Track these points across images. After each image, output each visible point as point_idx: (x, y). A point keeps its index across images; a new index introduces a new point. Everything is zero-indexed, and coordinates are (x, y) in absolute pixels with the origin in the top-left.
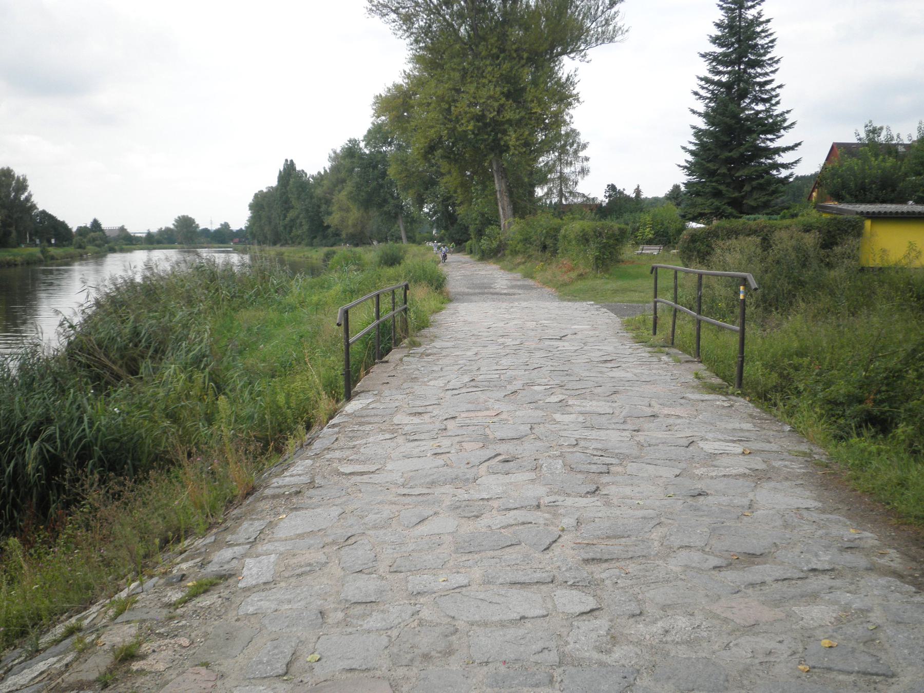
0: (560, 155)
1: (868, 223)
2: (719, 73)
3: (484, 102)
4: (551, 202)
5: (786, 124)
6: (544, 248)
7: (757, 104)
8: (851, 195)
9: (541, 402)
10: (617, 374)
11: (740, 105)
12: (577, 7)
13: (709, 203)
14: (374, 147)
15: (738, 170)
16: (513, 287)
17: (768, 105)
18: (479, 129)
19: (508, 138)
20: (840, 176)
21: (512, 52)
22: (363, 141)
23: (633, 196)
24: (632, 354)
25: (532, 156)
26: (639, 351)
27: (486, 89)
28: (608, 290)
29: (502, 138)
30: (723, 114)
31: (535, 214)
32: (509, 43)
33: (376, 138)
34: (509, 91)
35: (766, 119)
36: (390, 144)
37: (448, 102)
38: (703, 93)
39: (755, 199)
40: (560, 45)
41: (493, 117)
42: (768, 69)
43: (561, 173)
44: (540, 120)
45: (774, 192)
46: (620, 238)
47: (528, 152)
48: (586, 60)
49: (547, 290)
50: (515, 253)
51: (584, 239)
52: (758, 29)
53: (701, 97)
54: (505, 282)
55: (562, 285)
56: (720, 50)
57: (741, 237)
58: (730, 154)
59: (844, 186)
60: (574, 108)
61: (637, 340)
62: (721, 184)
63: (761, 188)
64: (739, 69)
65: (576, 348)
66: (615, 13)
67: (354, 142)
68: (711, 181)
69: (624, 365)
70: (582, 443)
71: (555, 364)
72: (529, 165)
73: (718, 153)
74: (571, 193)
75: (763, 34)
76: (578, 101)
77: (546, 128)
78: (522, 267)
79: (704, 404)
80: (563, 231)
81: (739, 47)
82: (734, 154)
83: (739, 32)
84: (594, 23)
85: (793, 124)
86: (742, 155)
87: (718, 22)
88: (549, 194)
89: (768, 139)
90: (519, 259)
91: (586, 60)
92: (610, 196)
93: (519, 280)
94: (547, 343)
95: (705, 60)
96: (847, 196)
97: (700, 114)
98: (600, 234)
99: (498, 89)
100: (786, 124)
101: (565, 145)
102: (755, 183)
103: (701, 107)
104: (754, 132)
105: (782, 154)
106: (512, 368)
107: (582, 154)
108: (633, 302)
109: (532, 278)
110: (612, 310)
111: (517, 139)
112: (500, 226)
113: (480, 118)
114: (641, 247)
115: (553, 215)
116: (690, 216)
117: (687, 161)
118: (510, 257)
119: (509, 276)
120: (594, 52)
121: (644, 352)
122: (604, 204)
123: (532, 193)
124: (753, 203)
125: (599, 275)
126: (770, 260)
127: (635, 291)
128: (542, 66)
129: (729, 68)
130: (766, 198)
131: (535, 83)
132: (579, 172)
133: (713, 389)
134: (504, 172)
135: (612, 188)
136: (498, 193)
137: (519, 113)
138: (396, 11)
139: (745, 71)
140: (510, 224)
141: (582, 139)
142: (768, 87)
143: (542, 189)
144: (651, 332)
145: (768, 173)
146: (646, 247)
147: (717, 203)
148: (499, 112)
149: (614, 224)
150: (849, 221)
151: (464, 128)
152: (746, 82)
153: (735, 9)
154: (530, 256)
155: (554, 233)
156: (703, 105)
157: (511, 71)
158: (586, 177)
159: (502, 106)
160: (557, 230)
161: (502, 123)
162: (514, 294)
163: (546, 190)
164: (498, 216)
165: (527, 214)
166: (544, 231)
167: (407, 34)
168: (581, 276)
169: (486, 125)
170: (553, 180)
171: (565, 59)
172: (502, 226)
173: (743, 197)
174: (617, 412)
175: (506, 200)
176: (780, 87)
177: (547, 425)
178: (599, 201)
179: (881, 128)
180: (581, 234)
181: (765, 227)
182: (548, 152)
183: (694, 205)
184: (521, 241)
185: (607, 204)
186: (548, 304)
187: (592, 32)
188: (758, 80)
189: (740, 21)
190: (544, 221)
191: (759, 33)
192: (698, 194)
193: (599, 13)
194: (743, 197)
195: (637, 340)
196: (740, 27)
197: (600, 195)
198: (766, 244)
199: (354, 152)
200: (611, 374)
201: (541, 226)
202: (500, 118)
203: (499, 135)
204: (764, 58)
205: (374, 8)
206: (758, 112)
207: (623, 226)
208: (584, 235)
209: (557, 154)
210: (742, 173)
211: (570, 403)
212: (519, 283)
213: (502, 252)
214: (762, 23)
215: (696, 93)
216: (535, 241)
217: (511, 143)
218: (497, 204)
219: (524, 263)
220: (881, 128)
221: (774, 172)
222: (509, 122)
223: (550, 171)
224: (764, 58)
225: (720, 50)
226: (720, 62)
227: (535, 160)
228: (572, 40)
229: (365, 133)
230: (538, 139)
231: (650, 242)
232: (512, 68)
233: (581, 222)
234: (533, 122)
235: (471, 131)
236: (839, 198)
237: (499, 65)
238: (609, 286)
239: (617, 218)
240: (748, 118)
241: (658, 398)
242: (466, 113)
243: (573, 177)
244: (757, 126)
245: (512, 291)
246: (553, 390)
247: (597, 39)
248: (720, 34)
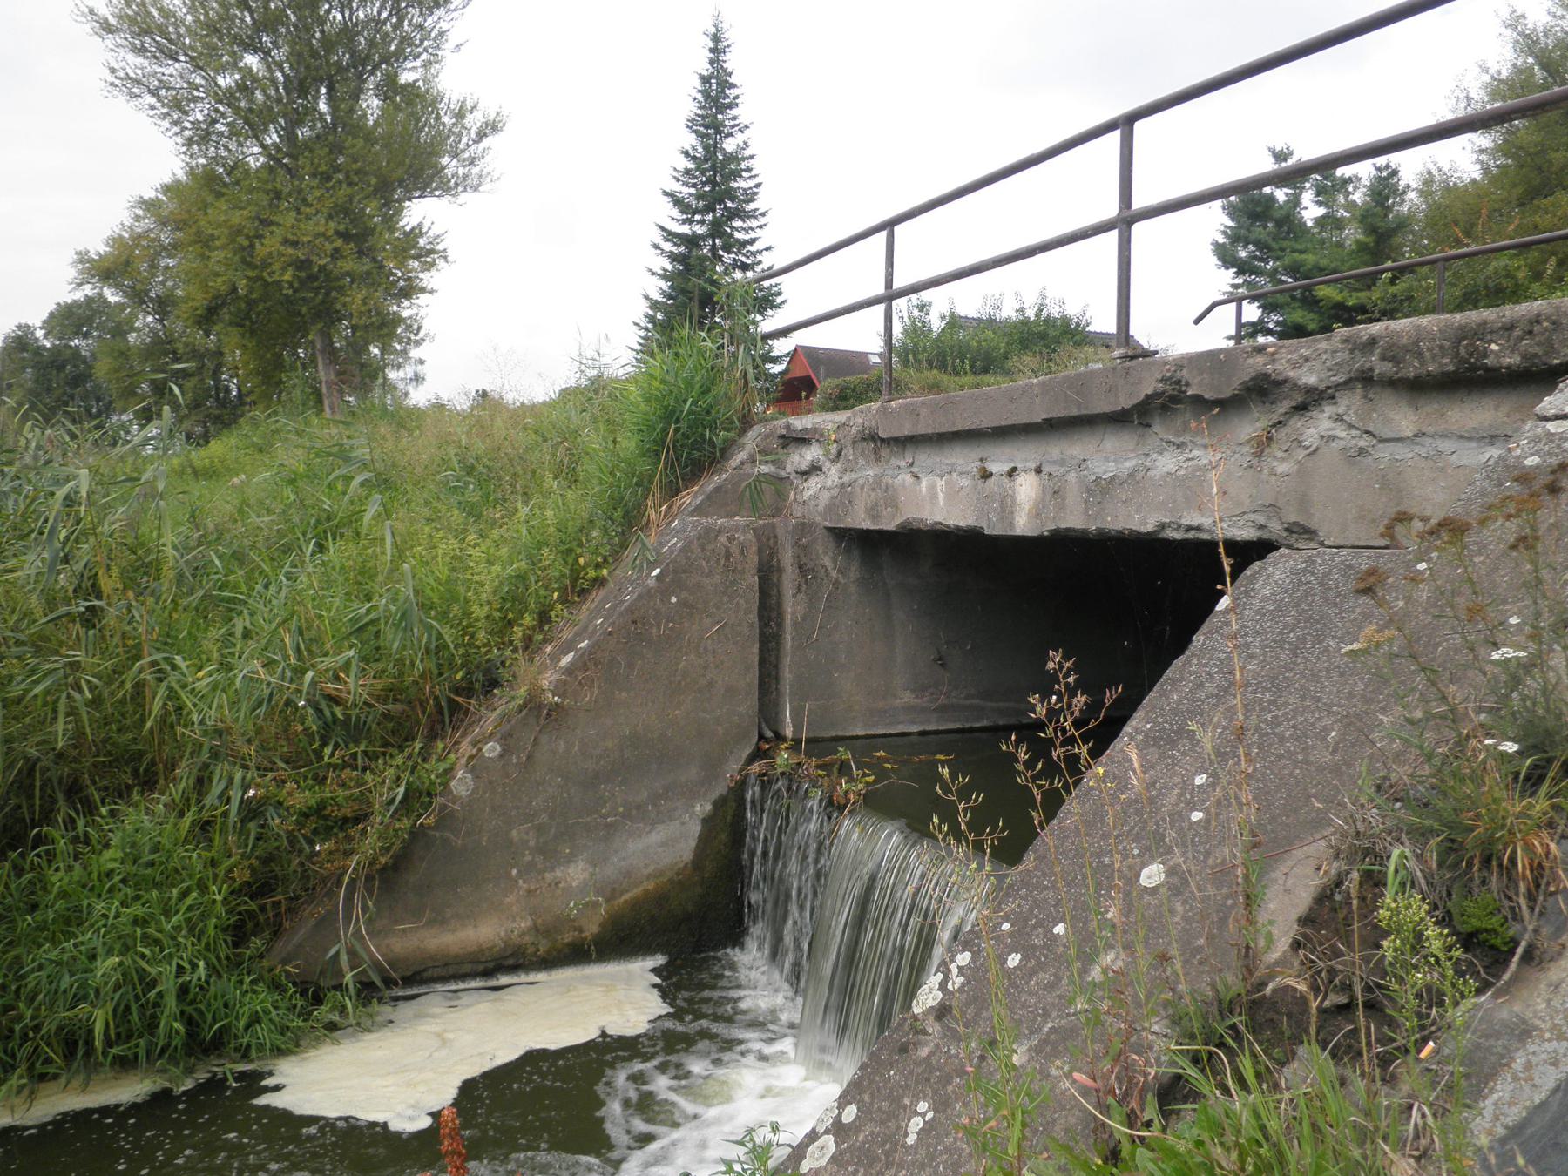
3: (309, 242)
14: (60, 339)
18: (302, 282)
19: (347, 299)
21: (352, 174)
22: (41, 328)
27: (311, 222)
33: (62, 325)
36: (86, 336)
37: (248, 237)
41: (325, 266)
42: (754, 223)
53: (663, 252)
67: (26, 329)
91: (459, 202)
99: (332, 225)
113: (302, 265)
136: (324, 385)
138: (154, 93)
151: (276, 277)
158: (420, 387)
167: (177, 129)
169: (312, 278)
176: (768, 249)
199: (27, 344)
203: (334, 294)
205: (118, 82)
215: (656, 247)
229: (45, 316)
235: (288, 282)
242: (281, 255)
243: (401, 385)
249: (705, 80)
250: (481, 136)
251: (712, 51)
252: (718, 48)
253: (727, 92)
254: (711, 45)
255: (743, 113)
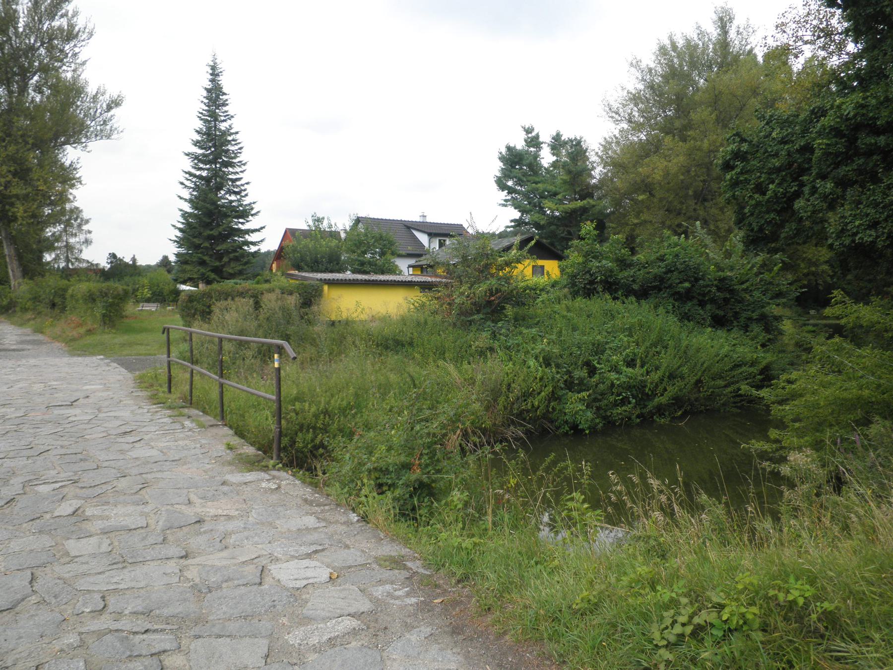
0: (65, 227)
1: (326, 288)
2: (200, 169)
4: (59, 266)
5: (253, 212)
6: (53, 305)
7: (230, 195)
8: (308, 266)
9: (48, 516)
10: (141, 452)
11: (217, 195)
12: (78, 106)
13: (196, 270)
15: (218, 245)
16: (22, 342)
17: (238, 197)
19: (16, 210)
20: (299, 252)
23: (131, 263)
24: (152, 420)
25: (40, 227)
26: (158, 416)
28: (116, 344)
29: (9, 210)
30: (204, 201)
31: (43, 276)
32: (15, 129)
34: (16, 170)
35: (238, 207)
38: (188, 183)
39: (233, 268)
40: (63, 136)
42: (238, 169)
43: (67, 242)
44: (46, 196)
45: (246, 263)
46: (123, 297)
47: (36, 223)
48: (87, 150)
49: (57, 344)
50: (25, 310)
51: (91, 298)
52: (230, 138)
53: (186, 186)
54: (15, 338)
55: (71, 340)
56: (201, 151)
57: (236, 299)
58: (211, 232)
59: (302, 259)
60: (77, 189)
61: (155, 402)
62: (204, 255)
63: (237, 259)
64: (216, 167)
65: (89, 417)
66: (112, 116)
68: (197, 253)
69: (146, 437)
70: (111, 600)
71: (66, 443)
72: (37, 235)
73: (202, 231)
74: (77, 259)
75: (233, 143)
76: (81, 184)
77: (52, 204)
78: (32, 322)
79: (249, 489)
80: (70, 291)
81: (215, 150)
82: (215, 233)
83: (215, 138)
84: (94, 122)
85: (258, 212)
86: (220, 234)
87: (198, 129)
88: (56, 259)
89: (239, 223)
90: (29, 315)
91: (87, 150)
92: (111, 262)
93: (29, 335)
94: (57, 411)
95: (188, 157)
96: (306, 267)
97: (186, 200)
98: (106, 294)
100: (253, 212)
101: (70, 219)
102: (232, 255)
103: (186, 194)
104: (229, 216)
105: (251, 234)
106: (11, 454)
107: (85, 227)
108: (140, 355)
109: (42, 333)
110: (122, 364)
111: (25, 212)
112: (10, 286)
114: (141, 304)
115: (61, 277)
116: (182, 280)
117: (177, 237)
118: (20, 313)
119: (20, 331)
120: (94, 145)
121: (163, 417)
122: (106, 269)
123: (41, 257)
124: (231, 271)
125: (106, 330)
126: (261, 317)
127: (141, 344)
128: (48, 152)
129: (208, 166)
130: (240, 268)
131: (41, 165)
132: (83, 242)
133: (251, 464)
134: (13, 240)
135: (113, 256)
137: (26, 189)
139: (220, 170)
140: (19, 284)
141: (85, 215)
142: (238, 183)
143: (50, 255)
144: (166, 390)
145: (241, 248)
146: (145, 304)
147: (202, 270)
148: (6, 188)
149: (118, 286)
150: (313, 286)
152: (222, 178)
153: (211, 121)
154: (39, 313)
155: (61, 293)
156: (188, 193)
157: (17, 153)
159: (9, 182)
160: (65, 290)
161: (10, 197)
162: (23, 350)
163: (53, 256)
164: (8, 277)
165: (36, 276)
166: (53, 291)
168: (90, 332)
170: (60, 248)
171: (68, 148)
172: (12, 286)
173: (223, 266)
174: (152, 522)
175: (15, 264)
176: (248, 183)
177: (57, 568)
178: (101, 267)
179: (323, 218)
180: (88, 294)
181: (250, 290)
182: (54, 224)
183: (184, 271)
184: (30, 299)
185: (109, 269)
186: (57, 361)
187: (92, 129)
188: (230, 177)
189: (215, 131)
190: (52, 282)
191: (229, 141)
192: (185, 262)
193: (98, 114)
194: (223, 266)
195: (155, 402)
196: (216, 135)
197: (104, 263)
198: (257, 305)
200: (134, 454)
201: (49, 286)
202: (7, 192)
203: (7, 207)
204: (234, 161)
206: (231, 202)
207: (125, 287)
208: (90, 295)
209: (62, 226)
210: (221, 247)
211: (89, 513)
212: (28, 338)
213: (13, 309)
214: (232, 134)
215: (182, 183)
216: (44, 299)
217: (19, 214)
218: (7, 267)
219: (34, 319)
220: (323, 218)
221: (246, 248)
222: (17, 196)
223: (57, 240)
224: (234, 161)
225: (201, 151)
226: (200, 161)
227: (42, 230)
228: (74, 133)
230: (44, 212)
231: (148, 301)
232: (18, 150)
233: (88, 283)
234: (40, 197)
236: (299, 268)
237: (5, 147)
238: (116, 341)
239: (119, 280)
240: (223, 206)
241: (197, 488)
243: (78, 246)
244: (232, 212)
245: (21, 346)
246: (65, 490)
247: (96, 135)
248: (200, 139)
249: (208, 91)
250: (109, 108)
251: (211, 74)
252: (215, 73)
253: (221, 97)
254: (211, 72)
255: (230, 109)
